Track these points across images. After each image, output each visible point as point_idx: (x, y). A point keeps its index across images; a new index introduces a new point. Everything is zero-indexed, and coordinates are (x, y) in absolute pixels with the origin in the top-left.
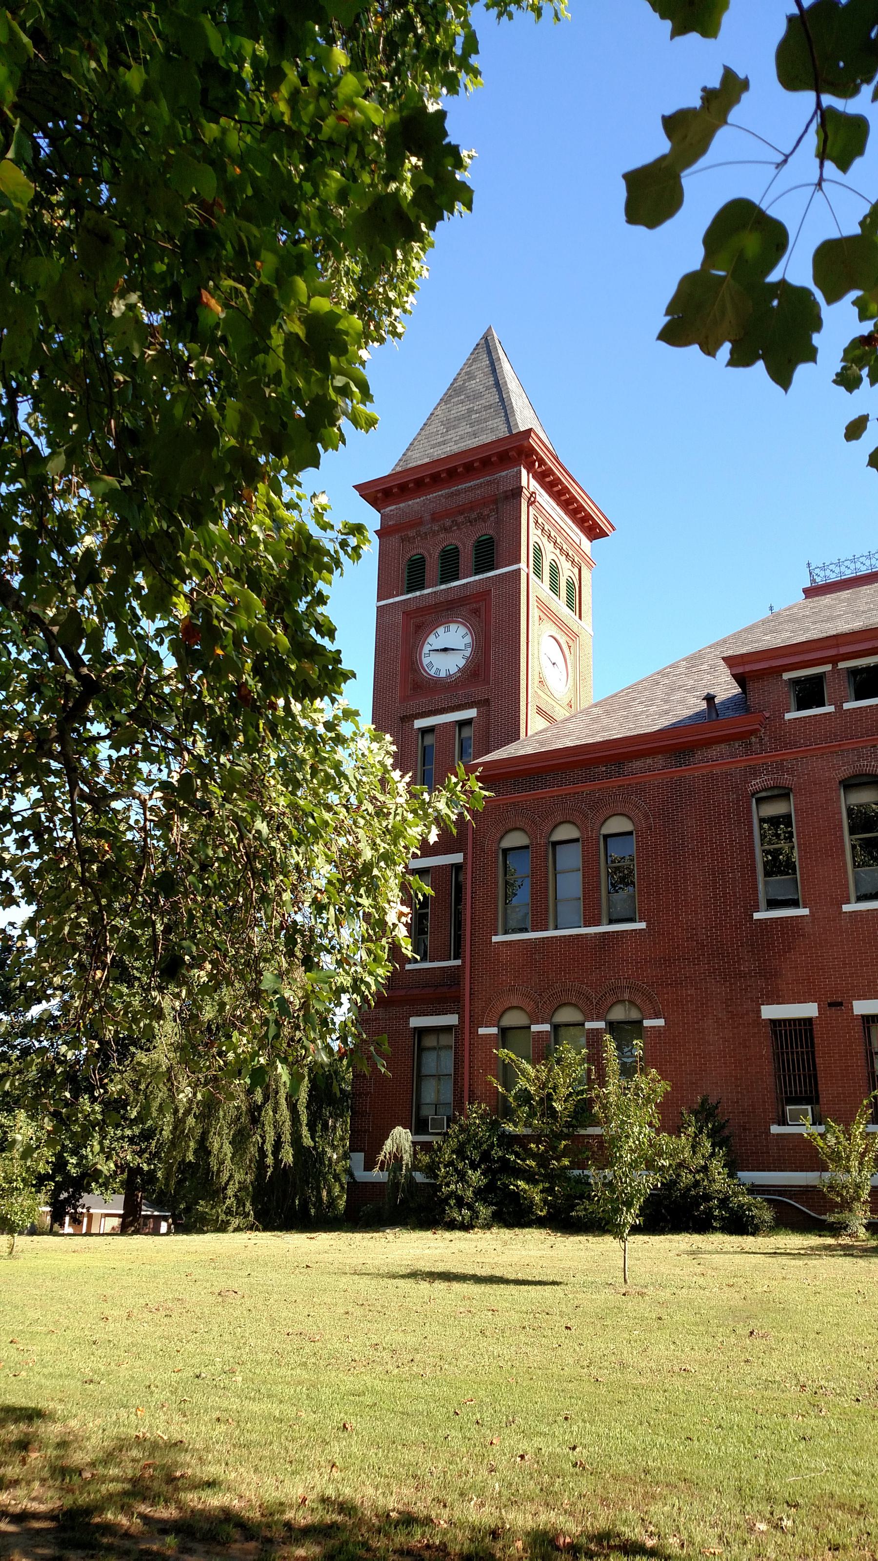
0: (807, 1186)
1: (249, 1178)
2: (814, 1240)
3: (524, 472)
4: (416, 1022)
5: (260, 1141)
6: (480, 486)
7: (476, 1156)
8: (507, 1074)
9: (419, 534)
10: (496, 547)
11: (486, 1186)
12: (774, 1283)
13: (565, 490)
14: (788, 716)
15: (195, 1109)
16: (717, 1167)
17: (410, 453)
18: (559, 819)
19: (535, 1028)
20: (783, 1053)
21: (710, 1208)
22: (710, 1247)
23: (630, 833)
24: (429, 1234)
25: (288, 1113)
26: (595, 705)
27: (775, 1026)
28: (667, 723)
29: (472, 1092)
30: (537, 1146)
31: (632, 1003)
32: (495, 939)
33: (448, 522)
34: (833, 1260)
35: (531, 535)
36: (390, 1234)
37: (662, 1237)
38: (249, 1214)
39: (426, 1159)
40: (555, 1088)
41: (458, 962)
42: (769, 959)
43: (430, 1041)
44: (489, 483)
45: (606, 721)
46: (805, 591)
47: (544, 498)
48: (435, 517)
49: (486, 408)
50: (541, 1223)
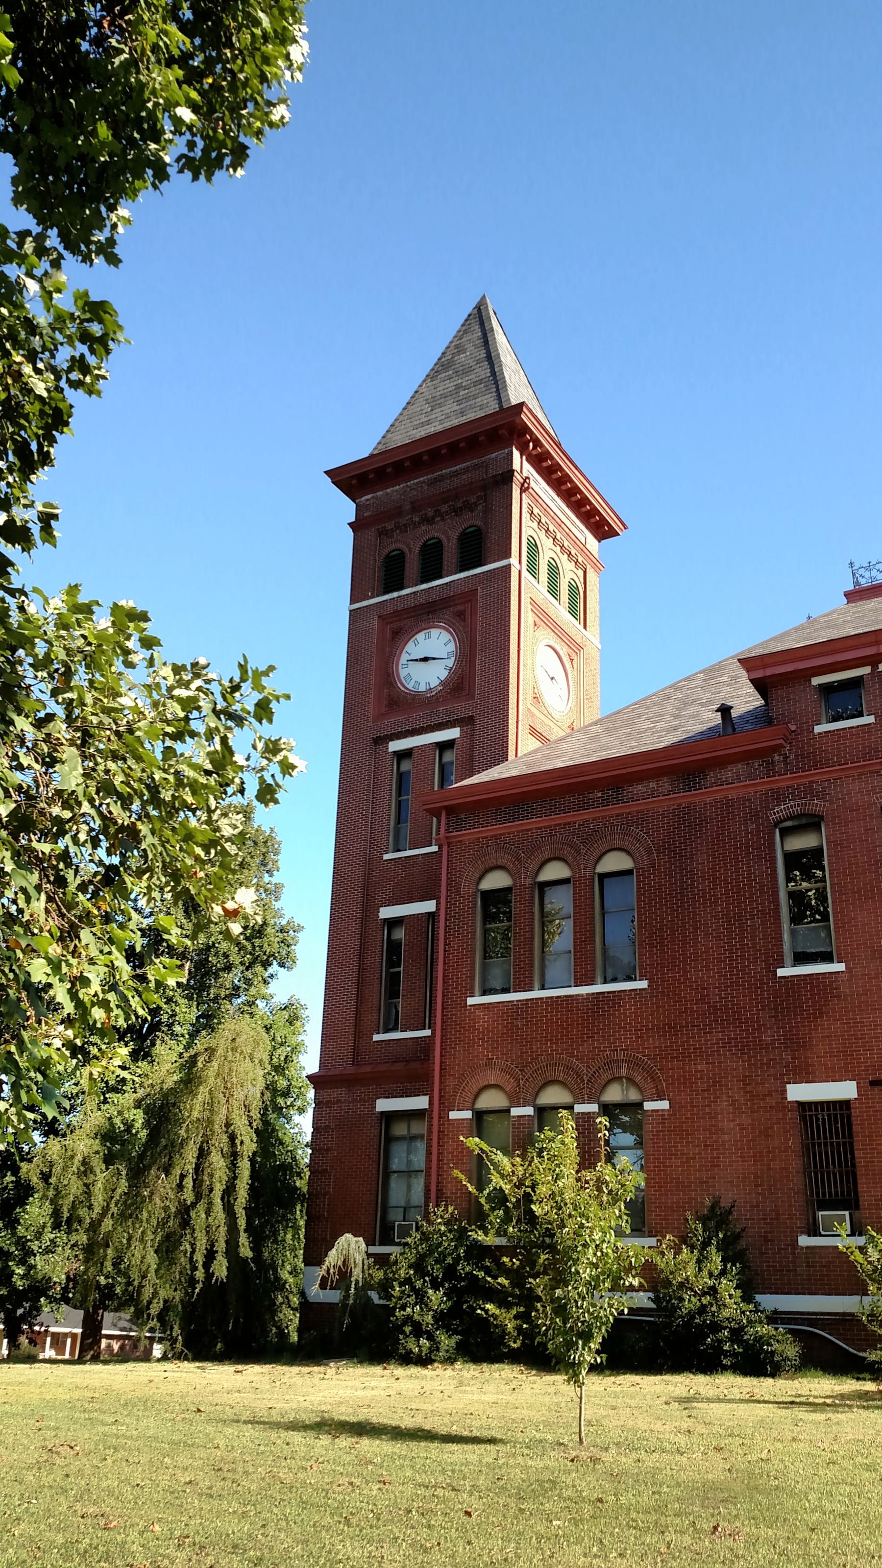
0: (844, 1314)
1: (178, 1295)
2: (850, 1385)
3: (516, 454)
4: (383, 1105)
5: (189, 1249)
6: (466, 470)
7: (438, 1272)
8: (480, 1170)
9: (397, 527)
10: (485, 540)
11: (449, 1309)
12: (779, 1445)
13: (566, 478)
14: (818, 729)
15: (114, 1209)
16: (728, 1288)
17: (389, 435)
19: (515, 1112)
20: (813, 1145)
21: (720, 1341)
22: (711, 1393)
23: (629, 872)
24: (377, 1370)
25: (223, 1216)
26: (595, 723)
27: (804, 1110)
28: (675, 740)
29: (440, 1192)
30: (511, 1260)
31: (630, 1080)
32: (471, 1001)
33: (430, 512)
34: (864, 1413)
35: (524, 526)
36: (331, 1369)
37: (659, 1377)
38: (176, 1339)
39: (379, 1275)
40: (533, 1187)
41: (427, 1032)
42: (796, 1026)
43: (400, 1129)
44: (476, 467)
45: (604, 740)
46: (847, 595)
47: (539, 485)
48: (415, 507)
49: (476, 384)
50: (514, 1358)
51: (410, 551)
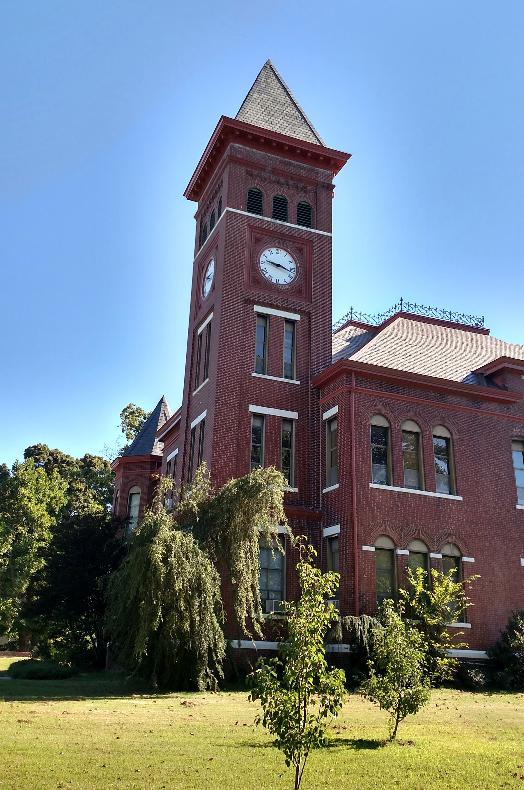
6: (305, 168)
18: (409, 417)
44: (311, 170)
48: (274, 171)
51: (292, 200)
